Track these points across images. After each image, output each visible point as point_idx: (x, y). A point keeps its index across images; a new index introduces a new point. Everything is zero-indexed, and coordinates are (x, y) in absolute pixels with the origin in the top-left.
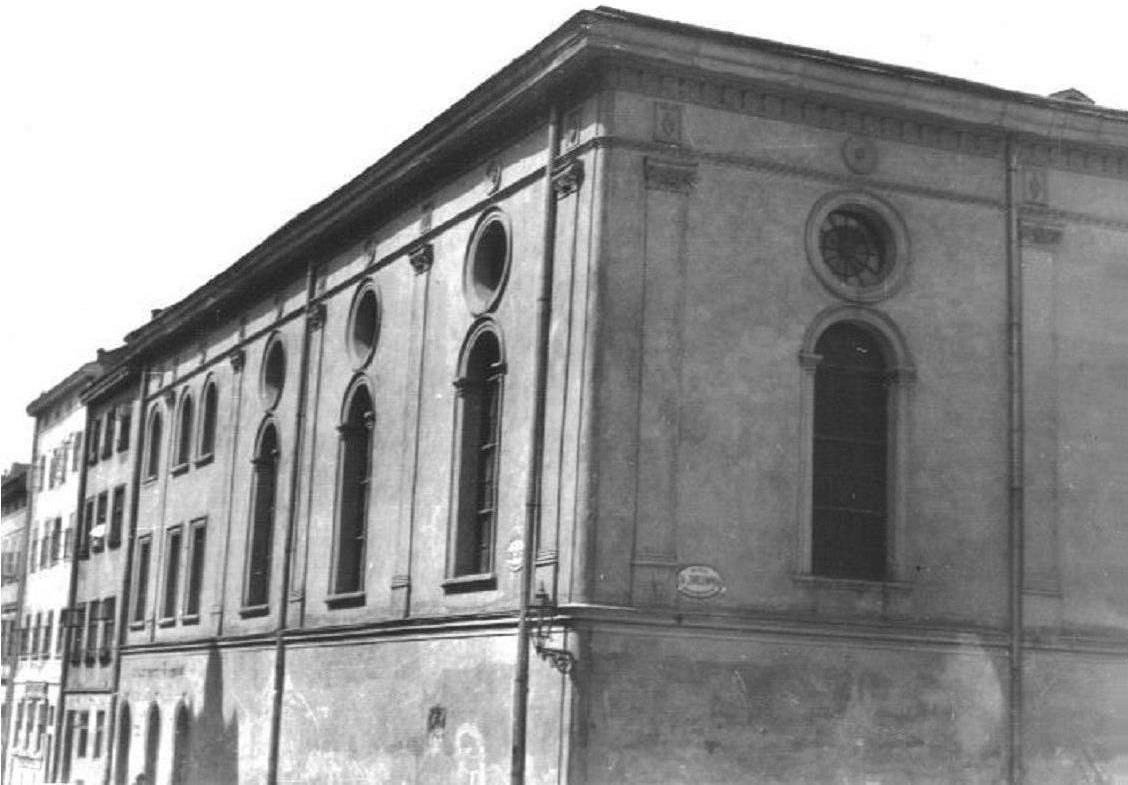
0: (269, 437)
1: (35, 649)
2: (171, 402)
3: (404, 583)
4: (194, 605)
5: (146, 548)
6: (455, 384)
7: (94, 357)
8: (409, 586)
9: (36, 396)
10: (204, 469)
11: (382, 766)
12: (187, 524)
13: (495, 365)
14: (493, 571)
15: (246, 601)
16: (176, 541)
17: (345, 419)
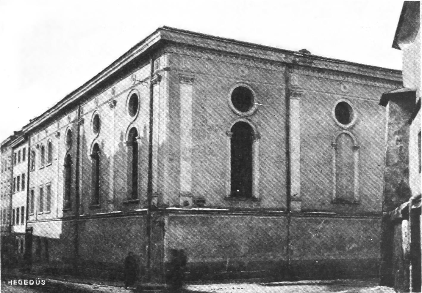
0: (68, 159)
4: (49, 208)
5: (33, 192)
11: (33, 268)
12: (45, 186)
16: (42, 189)
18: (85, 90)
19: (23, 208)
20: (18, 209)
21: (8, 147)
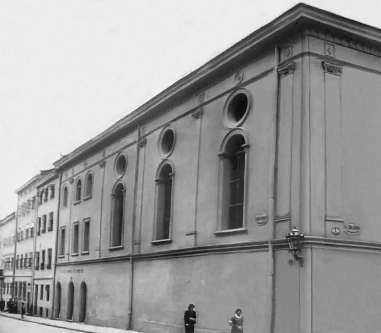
1: (21, 266)
2: (72, 182)
3: (98, 249)
4: (86, 247)
6: (156, 181)
7: (40, 173)
8: (100, 250)
9: (59, 158)
10: (86, 202)
13: (170, 174)
14: (246, 226)
15: (111, 245)
16: (77, 227)
17: (114, 193)
18: (313, 15)
19: (50, 250)
20: (44, 252)
21: (32, 188)
